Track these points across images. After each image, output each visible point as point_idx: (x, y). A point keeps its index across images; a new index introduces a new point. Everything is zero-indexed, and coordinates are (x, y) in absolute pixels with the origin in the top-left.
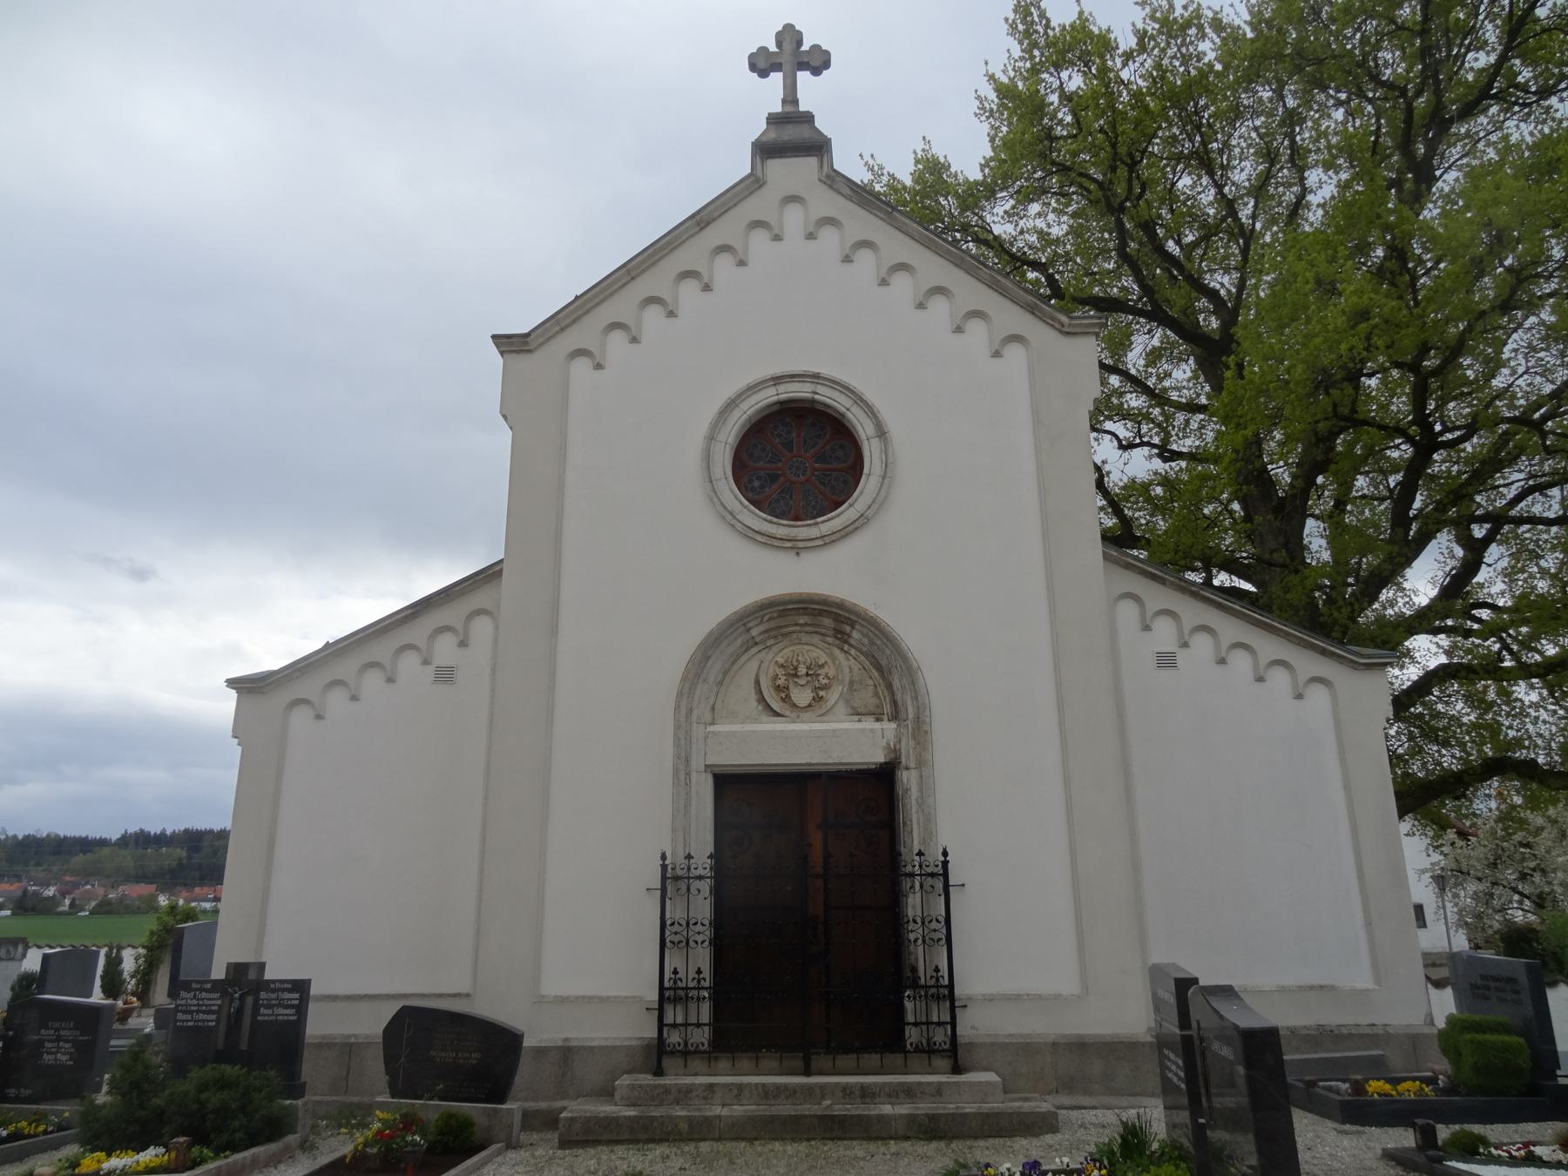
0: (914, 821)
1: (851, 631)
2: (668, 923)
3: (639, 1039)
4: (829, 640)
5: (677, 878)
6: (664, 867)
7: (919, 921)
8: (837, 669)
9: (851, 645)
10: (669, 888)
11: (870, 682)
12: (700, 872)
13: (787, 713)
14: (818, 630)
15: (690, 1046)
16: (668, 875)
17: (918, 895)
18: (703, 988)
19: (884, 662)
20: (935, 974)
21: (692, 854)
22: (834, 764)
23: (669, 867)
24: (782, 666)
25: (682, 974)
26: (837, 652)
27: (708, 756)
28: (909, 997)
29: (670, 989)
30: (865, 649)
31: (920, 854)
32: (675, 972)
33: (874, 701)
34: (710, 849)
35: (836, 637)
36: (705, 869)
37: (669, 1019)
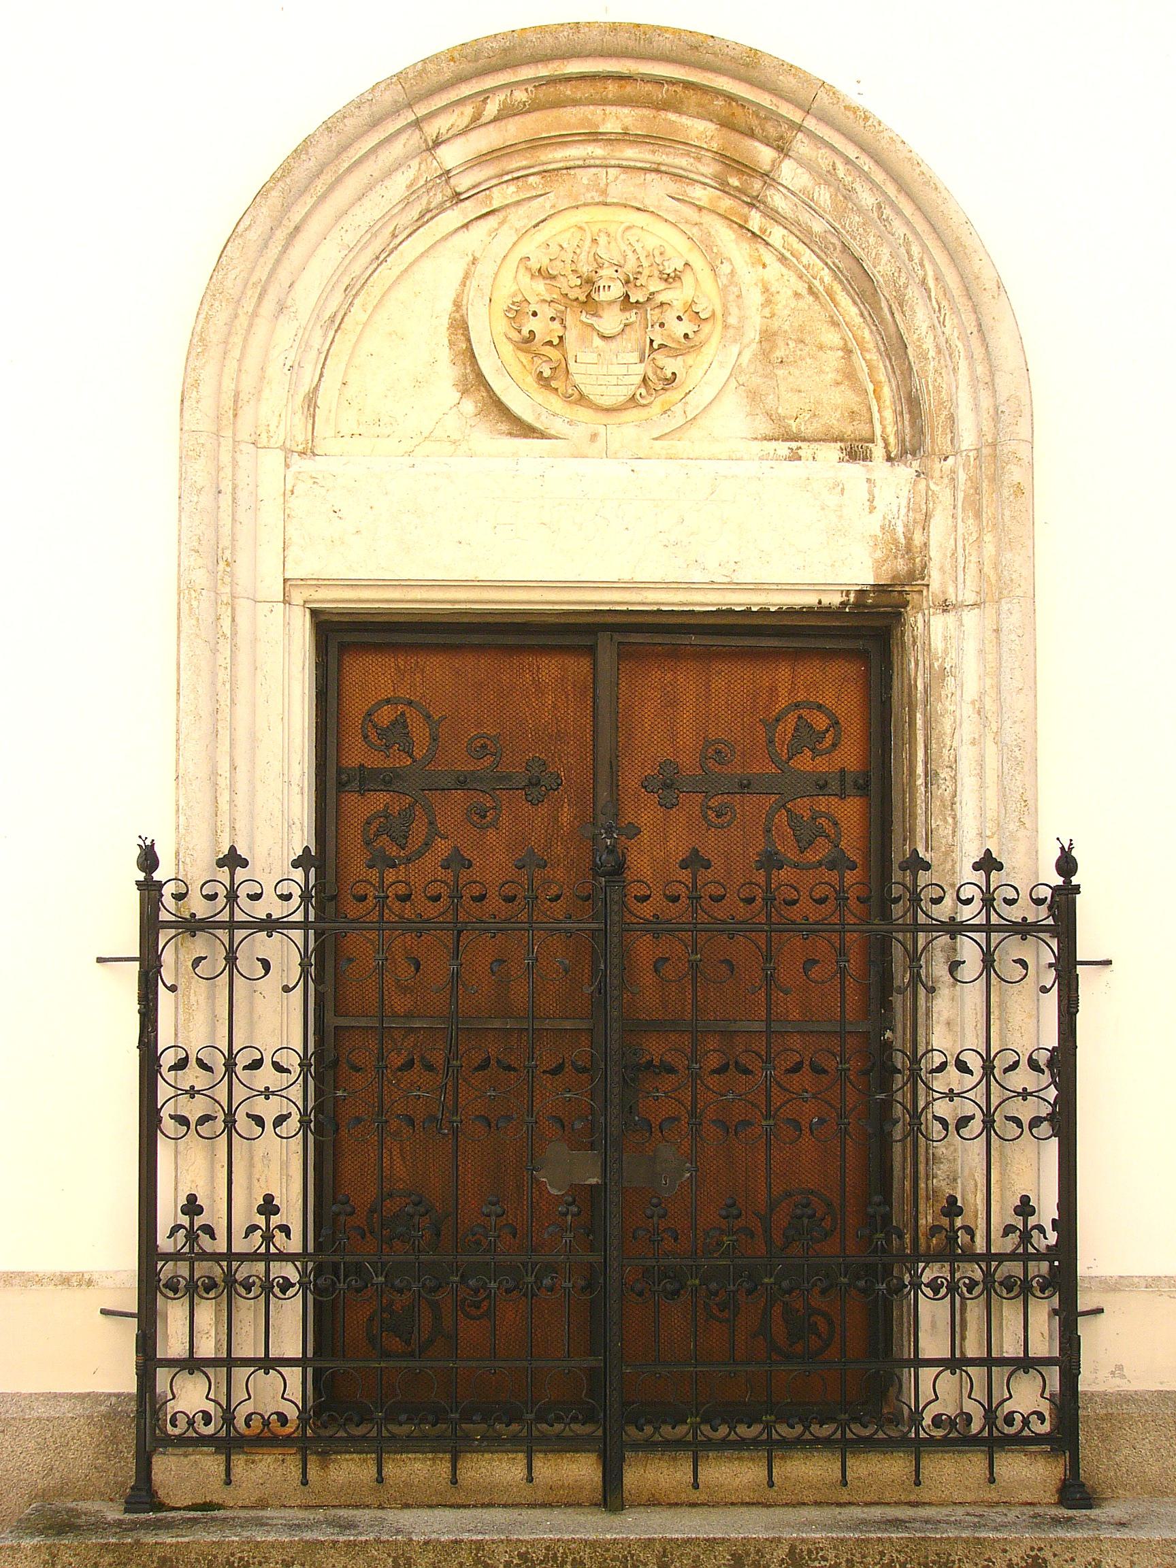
0: (966, 766)
1: (775, 165)
2: (168, 1060)
3: (82, 1397)
4: (700, 194)
5: (191, 926)
6: (150, 890)
7: (975, 1063)
8: (723, 291)
9: (773, 215)
10: (168, 957)
11: (831, 337)
12: (270, 907)
13: (556, 426)
14: (661, 157)
15: (240, 1423)
16: (164, 916)
17: (973, 995)
18: (283, 1257)
19: (882, 267)
20: (1018, 1222)
21: (242, 852)
22: (712, 586)
23: (168, 890)
24: (542, 274)
25: (214, 1215)
26: (725, 236)
27: (291, 553)
28: (934, 1286)
29: (176, 1256)
30: (818, 226)
31: (988, 863)
32: (192, 1207)
33: (843, 397)
34: (301, 838)
35: (724, 187)
36: (287, 897)
37: (173, 1344)
